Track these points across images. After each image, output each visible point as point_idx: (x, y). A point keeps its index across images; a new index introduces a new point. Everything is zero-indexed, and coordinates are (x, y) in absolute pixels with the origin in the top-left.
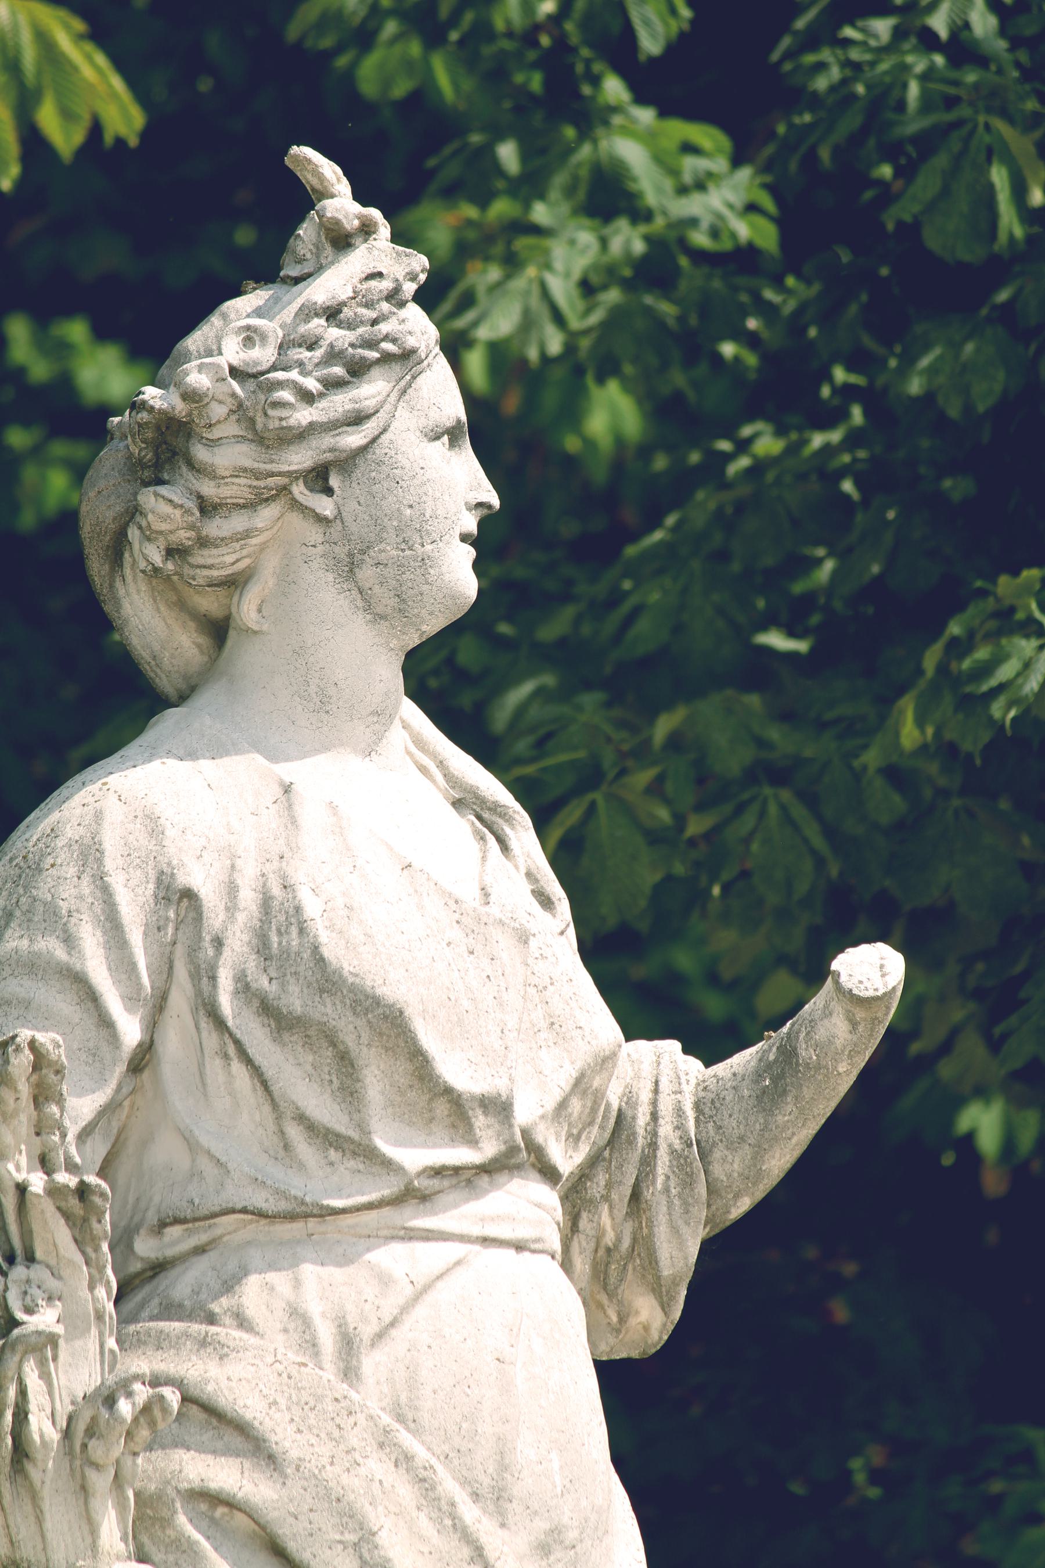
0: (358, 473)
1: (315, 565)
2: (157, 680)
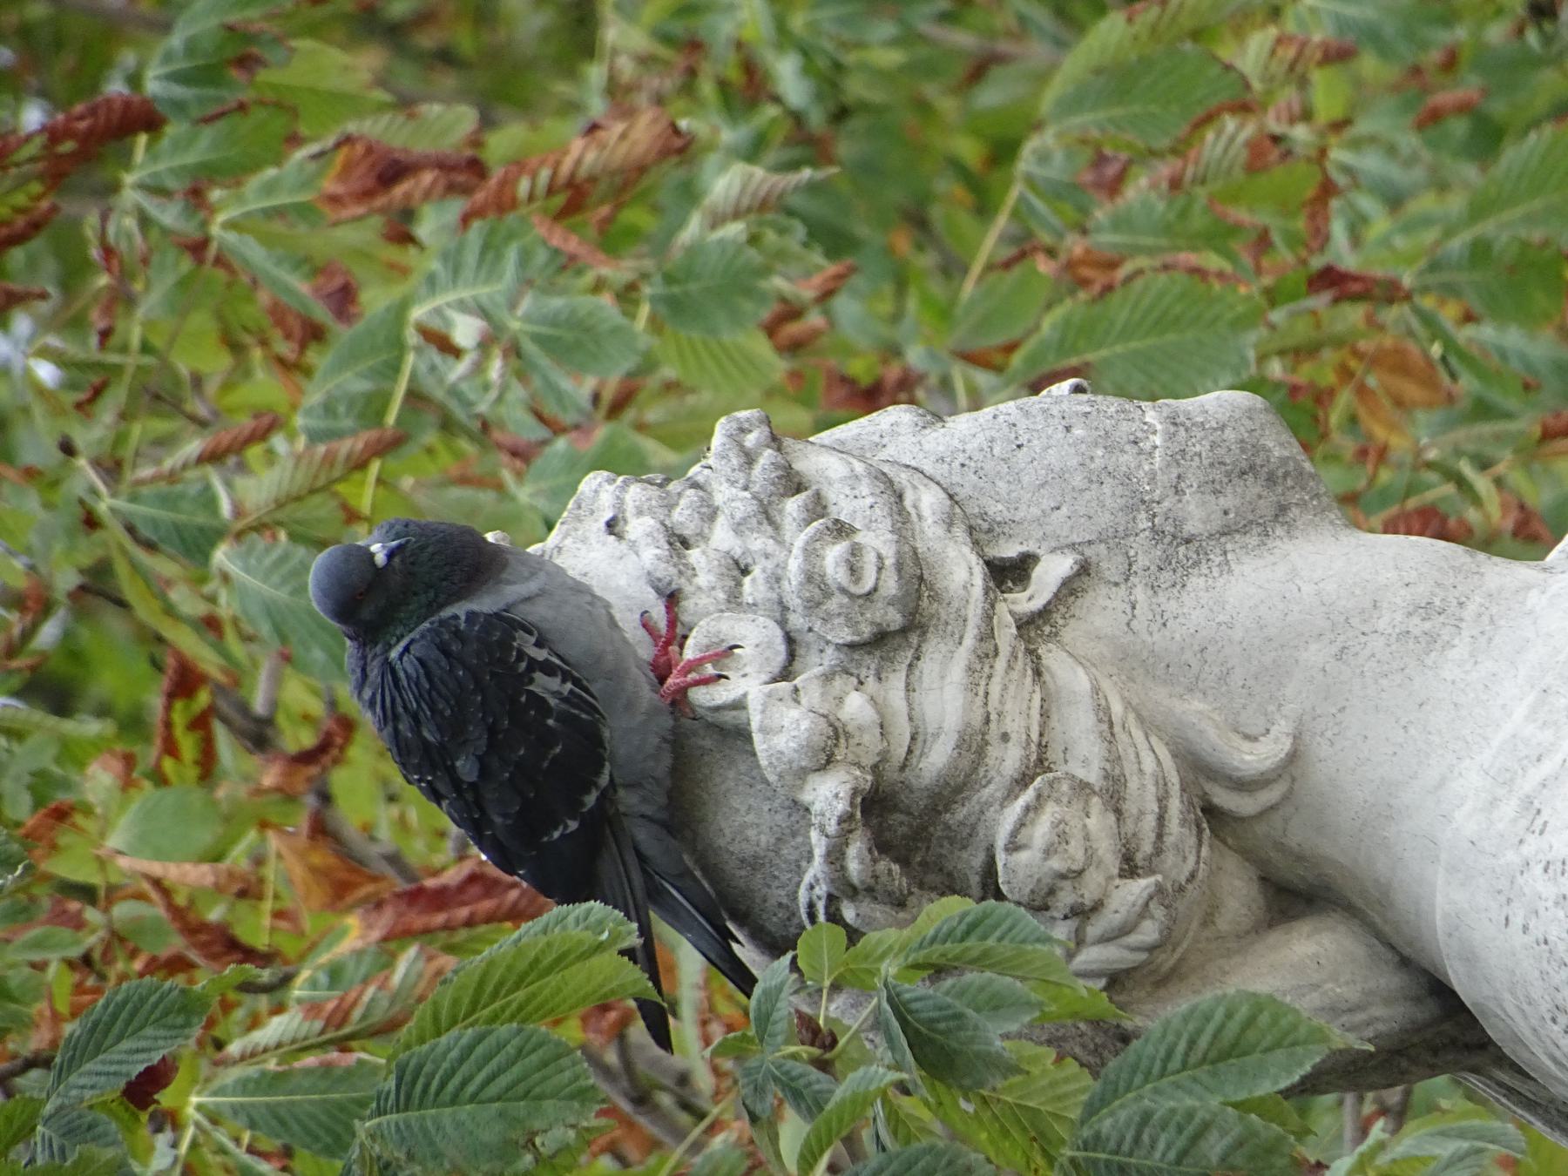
0: (996, 510)
1: (1171, 607)
2: (1381, 1027)
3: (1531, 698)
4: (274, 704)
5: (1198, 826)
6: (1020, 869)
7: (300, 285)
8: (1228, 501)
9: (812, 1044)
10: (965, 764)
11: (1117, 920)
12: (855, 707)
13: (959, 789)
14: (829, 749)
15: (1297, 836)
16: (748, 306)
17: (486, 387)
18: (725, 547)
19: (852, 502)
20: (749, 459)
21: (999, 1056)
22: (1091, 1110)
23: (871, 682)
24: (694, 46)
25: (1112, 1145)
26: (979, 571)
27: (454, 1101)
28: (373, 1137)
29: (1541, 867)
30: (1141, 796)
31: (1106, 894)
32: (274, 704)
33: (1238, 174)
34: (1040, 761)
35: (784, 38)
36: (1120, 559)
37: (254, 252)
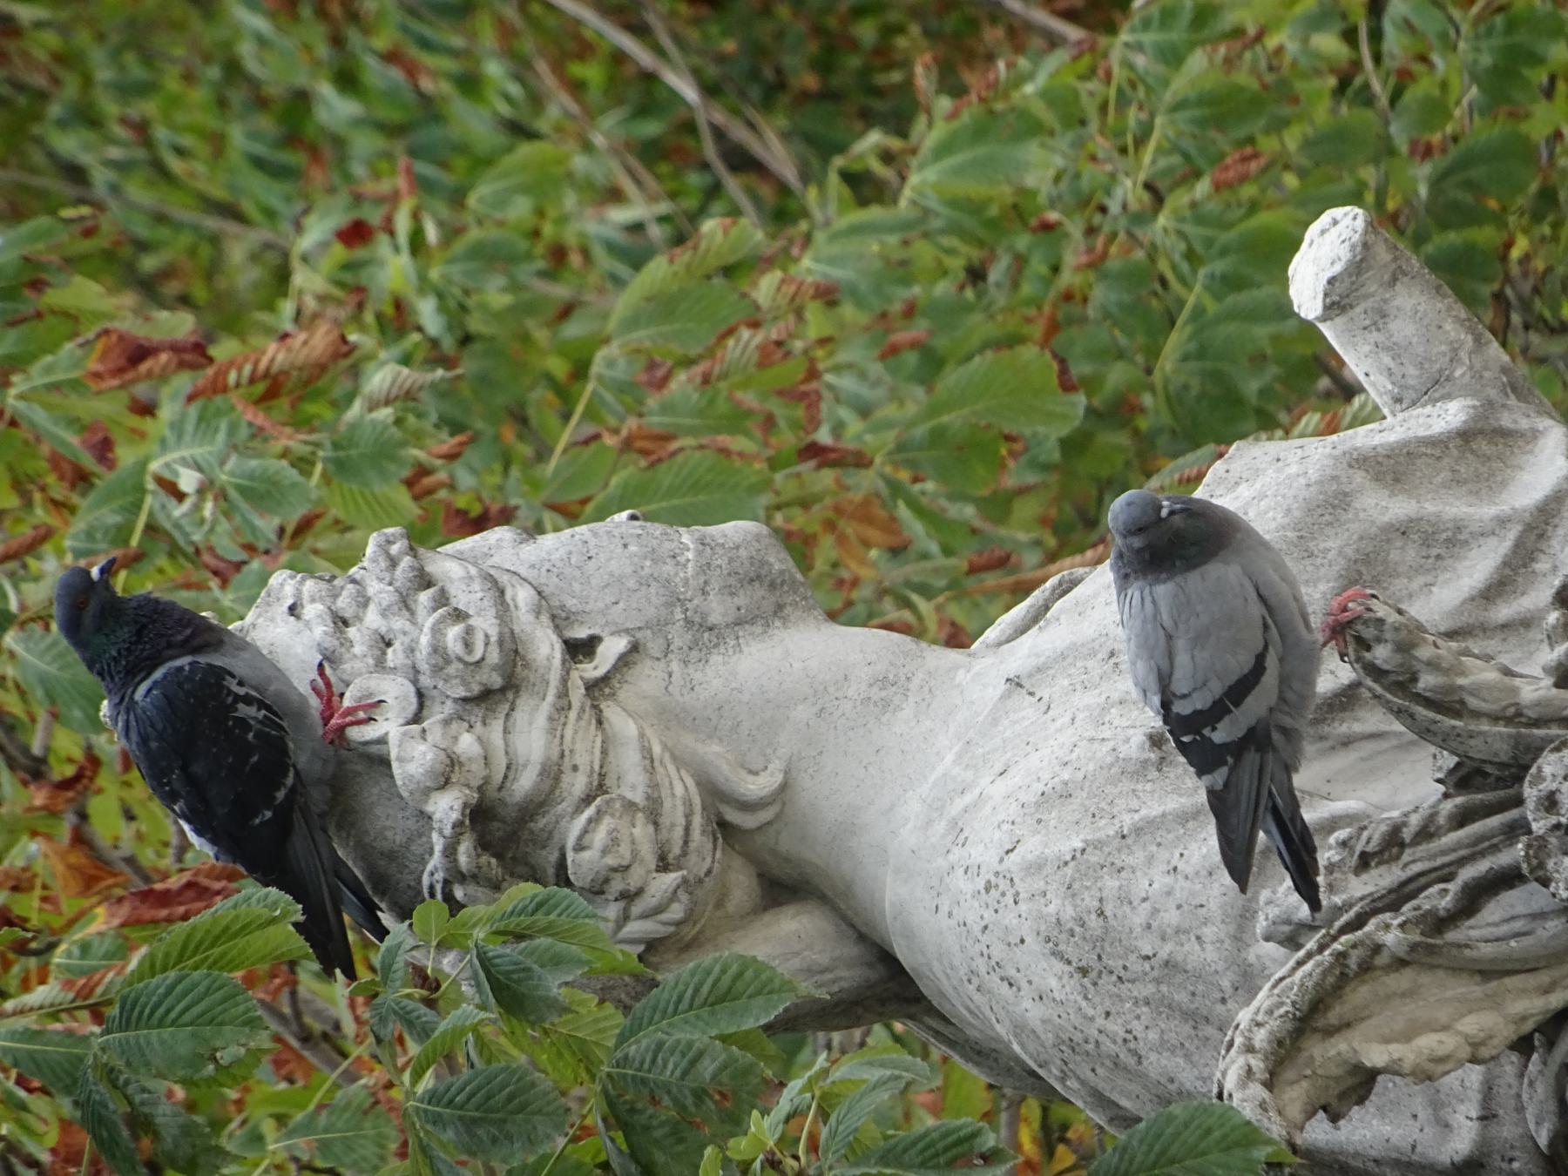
0: (571, 603)
1: (698, 676)
2: (844, 984)
3: (956, 749)
4: (47, 749)
5: (714, 835)
6: (583, 864)
7: (73, 439)
8: (741, 600)
9: (422, 987)
10: (546, 786)
11: (654, 902)
12: (467, 744)
13: (541, 804)
14: (447, 773)
15: (786, 843)
16: (393, 468)
17: (202, 521)
18: (374, 626)
19: (467, 596)
20: (393, 563)
21: (556, 1000)
22: (622, 1039)
23: (478, 727)
24: (359, 290)
25: (637, 1064)
26: (559, 647)
27: (160, 1025)
28: (103, 1050)
29: (962, 870)
30: (674, 813)
31: (646, 883)
32: (47, 749)
33: (752, 369)
34: (601, 786)
35: (424, 286)
36: (661, 640)
37: (40, 416)
